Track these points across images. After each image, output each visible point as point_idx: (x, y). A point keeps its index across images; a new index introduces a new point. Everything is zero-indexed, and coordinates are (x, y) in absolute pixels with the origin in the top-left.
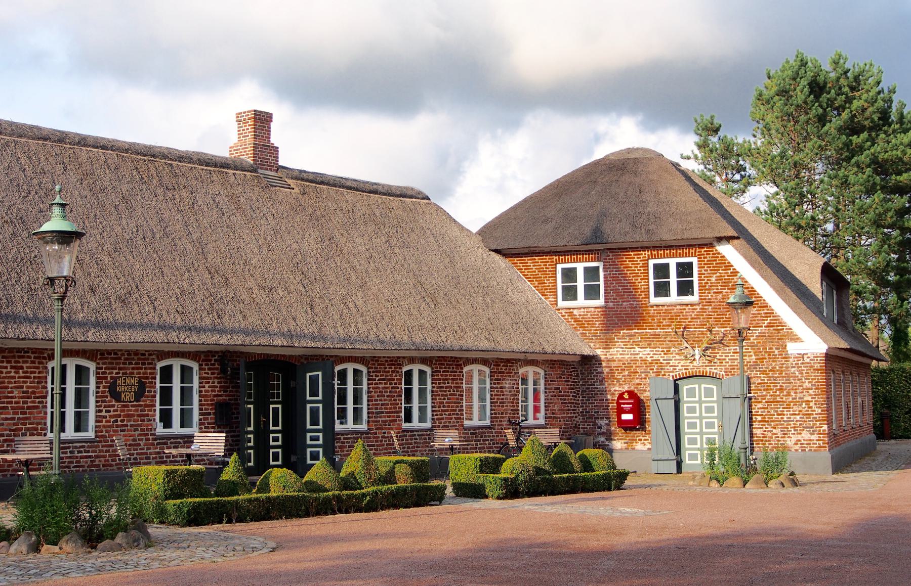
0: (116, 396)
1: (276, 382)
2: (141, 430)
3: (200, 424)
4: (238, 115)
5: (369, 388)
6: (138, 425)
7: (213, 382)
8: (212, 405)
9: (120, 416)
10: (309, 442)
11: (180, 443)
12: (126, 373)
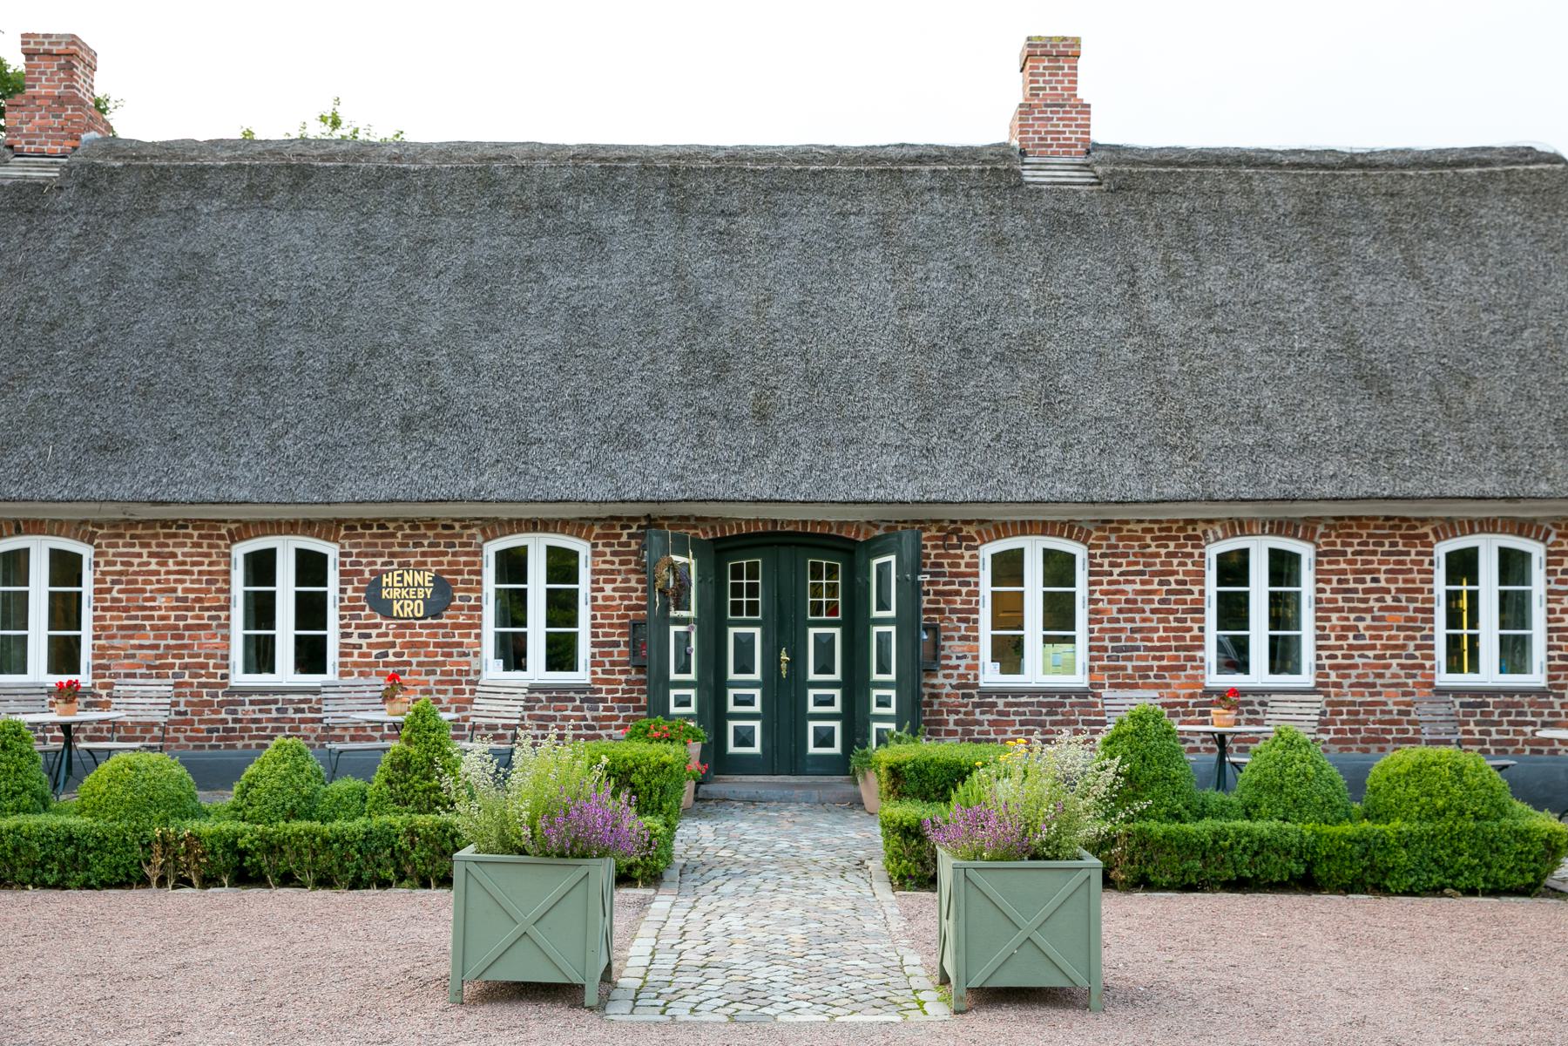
1: (822, 586)
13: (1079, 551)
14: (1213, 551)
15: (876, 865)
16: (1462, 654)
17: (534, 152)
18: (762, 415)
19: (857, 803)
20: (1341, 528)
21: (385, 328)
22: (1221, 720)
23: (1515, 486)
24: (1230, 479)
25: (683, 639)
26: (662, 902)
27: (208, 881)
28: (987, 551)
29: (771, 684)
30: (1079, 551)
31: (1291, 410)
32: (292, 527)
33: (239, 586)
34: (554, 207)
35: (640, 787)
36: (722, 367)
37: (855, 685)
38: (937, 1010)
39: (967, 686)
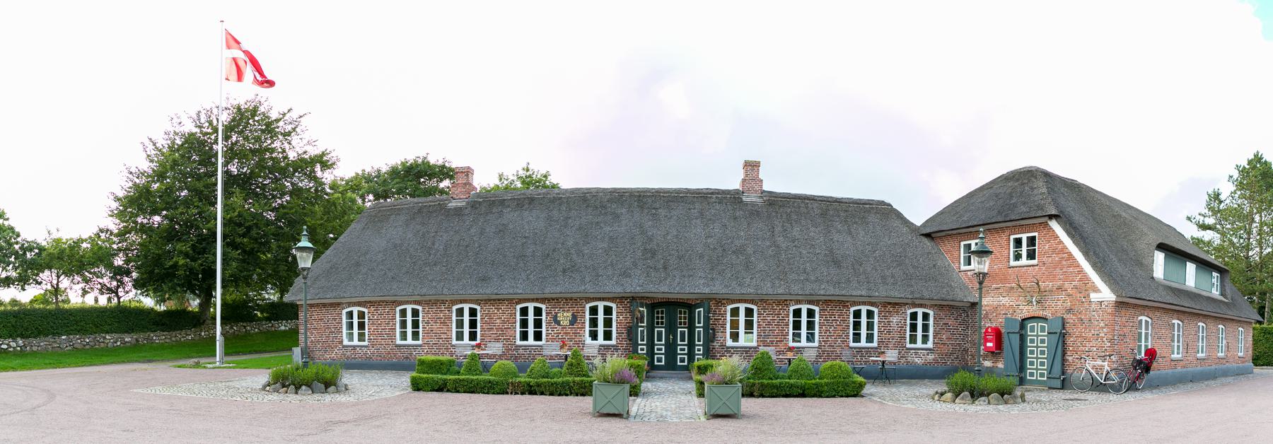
0: (558, 323)
1: (682, 317)
4: (1258, 158)
13: (755, 308)
14: (792, 308)
15: (694, 392)
16: (857, 337)
17: (599, 190)
18: (665, 268)
19: (691, 378)
20: (826, 303)
21: (557, 243)
22: (790, 355)
23: (870, 293)
24: (796, 289)
25: (642, 332)
26: (639, 400)
27: (523, 393)
28: (729, 308)
29: (667, 345)
30: (755, 308)
31: (814, 270)
32: (533, 300)
33: (518, 317)
34: (605, 207)
35: (638, 370)
36: (654, 253)
37: (691, 345)
38: (703, 419)
39: (723, 345)
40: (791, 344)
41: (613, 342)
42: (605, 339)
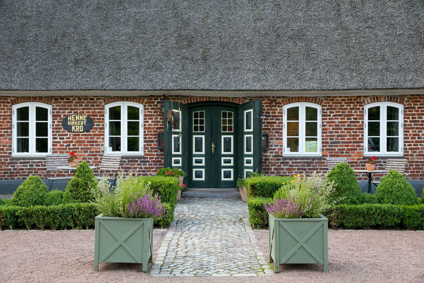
0: (69, 128)
2: (90, 152)
3: (145, 149)
5: (323, 122)
6: (88, 148)
7: (157, 118)
8: (155, 135)
9: (72, 142)
10: (223, 164)
11: (125, 162)
12: (77, 112)
13: (319, 108)
14: (367, 107)
15: (246, 220)
18: (205, 59)
19: (239, 198)
22: (370, 168)
24: (373, 81)
25: (177, 139)
26: (170, 234)
28: (286, 108)
30: (319, 108)
31: (396, 56)
32: (34, 99)
33: (15, 121)
36: (190, 42)
37: (238, 156)
38: (269, 272)
39: (278, 156)
40: (367, 153)
41: (140, 153)
42: (129, 149)
